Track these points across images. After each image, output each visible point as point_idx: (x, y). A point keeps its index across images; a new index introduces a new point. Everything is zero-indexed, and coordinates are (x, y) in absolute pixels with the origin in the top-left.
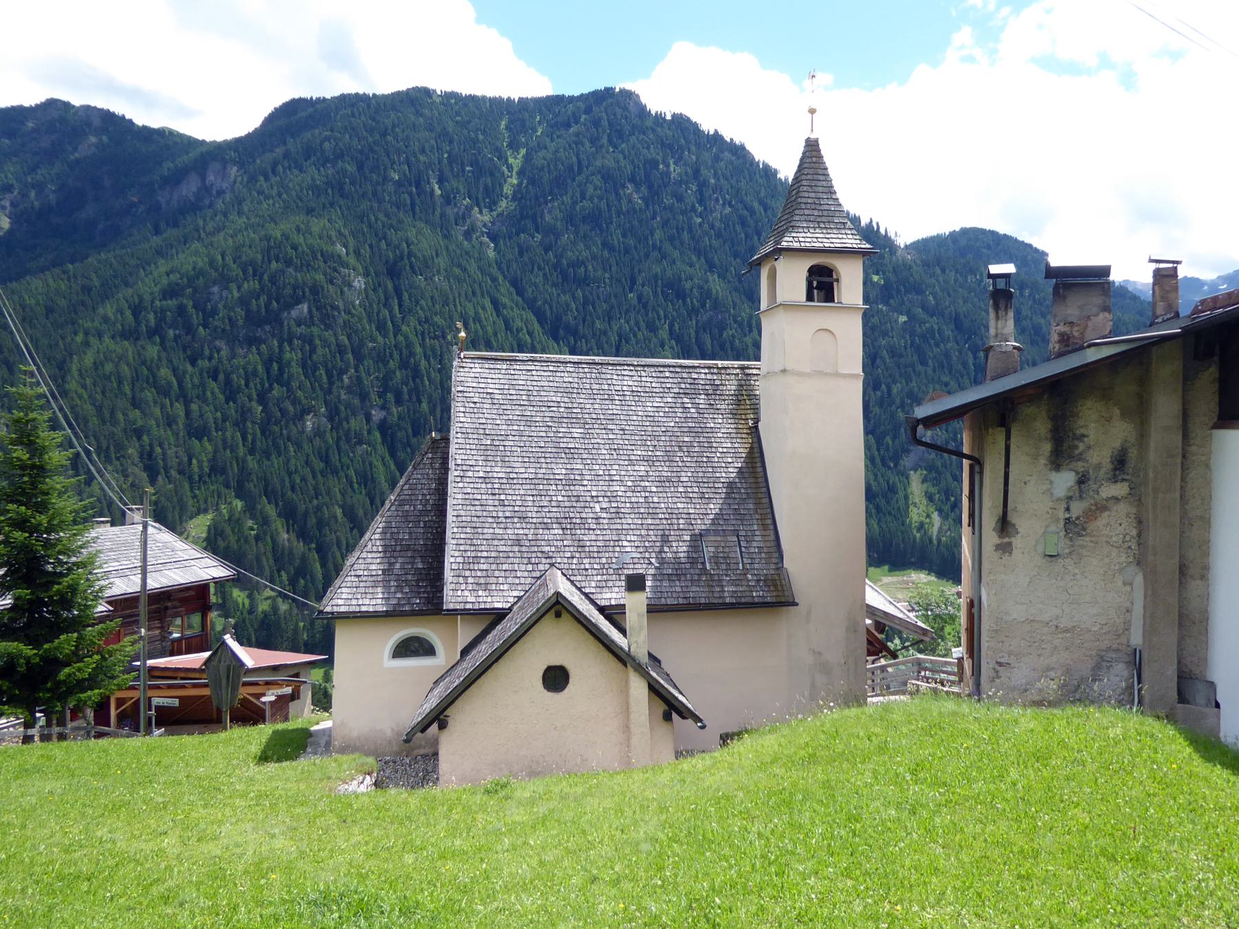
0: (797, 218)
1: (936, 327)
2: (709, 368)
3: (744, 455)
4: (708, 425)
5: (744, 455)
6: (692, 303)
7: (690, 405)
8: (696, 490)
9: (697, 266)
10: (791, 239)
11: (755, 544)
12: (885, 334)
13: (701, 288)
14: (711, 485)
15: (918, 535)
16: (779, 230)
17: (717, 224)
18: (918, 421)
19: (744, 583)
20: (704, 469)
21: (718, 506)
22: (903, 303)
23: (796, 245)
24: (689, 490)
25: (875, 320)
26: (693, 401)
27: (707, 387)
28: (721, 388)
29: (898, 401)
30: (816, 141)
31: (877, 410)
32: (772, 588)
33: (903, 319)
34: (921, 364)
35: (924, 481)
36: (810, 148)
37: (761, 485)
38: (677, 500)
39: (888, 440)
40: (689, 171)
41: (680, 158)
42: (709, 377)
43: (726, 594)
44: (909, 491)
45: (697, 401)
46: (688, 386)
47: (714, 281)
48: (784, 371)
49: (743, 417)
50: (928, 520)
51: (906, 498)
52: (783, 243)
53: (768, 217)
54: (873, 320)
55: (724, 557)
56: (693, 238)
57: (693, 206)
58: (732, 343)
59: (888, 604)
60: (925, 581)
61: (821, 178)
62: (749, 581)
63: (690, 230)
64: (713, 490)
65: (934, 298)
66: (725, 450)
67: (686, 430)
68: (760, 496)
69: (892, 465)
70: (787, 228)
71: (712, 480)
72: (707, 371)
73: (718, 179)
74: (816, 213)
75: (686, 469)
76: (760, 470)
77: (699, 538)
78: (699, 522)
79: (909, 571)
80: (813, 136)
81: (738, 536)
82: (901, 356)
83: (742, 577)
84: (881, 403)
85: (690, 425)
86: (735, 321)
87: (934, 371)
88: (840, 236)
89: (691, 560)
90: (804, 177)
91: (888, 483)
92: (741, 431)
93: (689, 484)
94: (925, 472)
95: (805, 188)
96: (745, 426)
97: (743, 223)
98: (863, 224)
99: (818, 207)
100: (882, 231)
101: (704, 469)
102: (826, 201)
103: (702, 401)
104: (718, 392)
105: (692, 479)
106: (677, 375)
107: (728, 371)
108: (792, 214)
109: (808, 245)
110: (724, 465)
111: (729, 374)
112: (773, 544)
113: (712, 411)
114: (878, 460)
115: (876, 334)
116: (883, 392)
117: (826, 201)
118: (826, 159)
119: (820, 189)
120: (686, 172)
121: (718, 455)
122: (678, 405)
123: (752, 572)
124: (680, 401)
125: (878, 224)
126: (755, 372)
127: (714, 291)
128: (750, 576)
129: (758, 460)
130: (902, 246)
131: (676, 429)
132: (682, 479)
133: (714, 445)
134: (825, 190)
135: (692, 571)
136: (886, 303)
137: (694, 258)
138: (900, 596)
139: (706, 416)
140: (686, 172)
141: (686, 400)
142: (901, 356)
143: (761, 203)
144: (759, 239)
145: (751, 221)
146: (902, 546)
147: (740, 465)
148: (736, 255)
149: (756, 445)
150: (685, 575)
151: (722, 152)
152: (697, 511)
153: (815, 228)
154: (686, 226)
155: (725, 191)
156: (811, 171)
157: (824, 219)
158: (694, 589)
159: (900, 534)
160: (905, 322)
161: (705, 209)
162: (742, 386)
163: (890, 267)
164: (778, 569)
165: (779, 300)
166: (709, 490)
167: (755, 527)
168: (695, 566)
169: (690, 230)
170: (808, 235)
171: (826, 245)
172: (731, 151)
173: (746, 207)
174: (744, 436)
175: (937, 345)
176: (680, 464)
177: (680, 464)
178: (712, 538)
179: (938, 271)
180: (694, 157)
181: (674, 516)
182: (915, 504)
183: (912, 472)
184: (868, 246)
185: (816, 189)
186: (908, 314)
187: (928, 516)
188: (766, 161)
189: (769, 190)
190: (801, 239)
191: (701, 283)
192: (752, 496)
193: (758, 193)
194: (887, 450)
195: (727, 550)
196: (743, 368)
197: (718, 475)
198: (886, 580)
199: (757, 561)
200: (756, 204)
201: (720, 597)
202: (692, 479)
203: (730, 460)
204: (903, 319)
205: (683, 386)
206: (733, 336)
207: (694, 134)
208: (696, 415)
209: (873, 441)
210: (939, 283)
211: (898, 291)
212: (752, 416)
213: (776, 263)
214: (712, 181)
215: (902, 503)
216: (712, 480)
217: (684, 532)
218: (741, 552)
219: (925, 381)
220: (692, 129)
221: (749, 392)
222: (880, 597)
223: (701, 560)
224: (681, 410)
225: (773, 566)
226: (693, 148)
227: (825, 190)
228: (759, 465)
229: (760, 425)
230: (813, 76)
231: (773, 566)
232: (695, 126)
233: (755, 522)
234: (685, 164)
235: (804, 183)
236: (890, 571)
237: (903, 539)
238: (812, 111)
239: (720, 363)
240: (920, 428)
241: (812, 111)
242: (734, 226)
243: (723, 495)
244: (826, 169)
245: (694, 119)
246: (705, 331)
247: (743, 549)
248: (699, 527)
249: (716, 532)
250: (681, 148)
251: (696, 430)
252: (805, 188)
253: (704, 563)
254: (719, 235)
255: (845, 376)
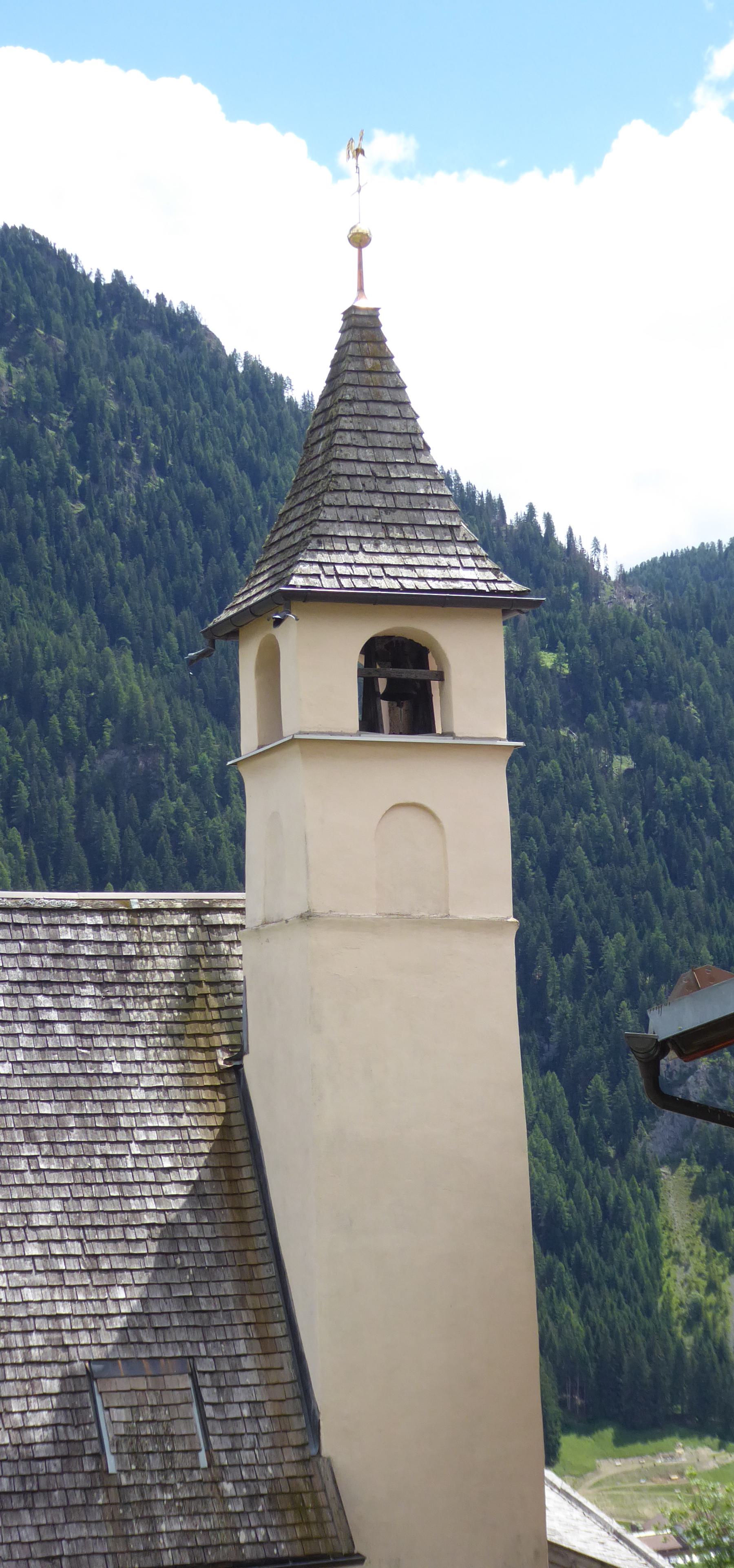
0: (330, 514)
1: (708, 784)
2: (106, 911)
3: (205, 1148)
4: (106, 1069)
5: (205, 1148)
6: (64, 727)
7: (54, 1015)
8: (75, 1248)
9: (77, 630)
10: (315, 569)
11: (240, 1395)
12: (578, 803)
13: (87, 687)
14: (116, 1234)
15: (688, 1341)
16: (284, 545)
17: (128, 519)
18: (663, 1047)
19: (214, 1506)
20: (95, 1191)
21: (137, 1292)
22: (622, 722)
23: (329, 584)
24: (57, 1250)
25: (551, 768)
26: (64, 1003)
27: (101, 964)
28: (139, 964)
29: (619, 980)
30: (373, 316)
31: (566, 1005)
32: (291, 1517)
33: (623, 763)
34: (674, 878)
35: (697, 1192)
36: (356, 335)
37: (254, 1229)
38: (21, 1280)
39: (599, 1083)
40: (50, 378)
41: (25, 346)
42: (106, 935)
43: (164, 1542)
44: (659, 1222)
45: (74, 1002)
46: (48, 962)
47: (124, 669)
48: (307, 917)
49: (202, 1042)
50: (712, 1299)
51: (653, 1238)
52: (295, 581)
53: (262, 500)
54: (547, 769)
55: (154, 1437)
56: (63, 554)
57: (62, 471)
58: (175, 834)
59: (611, 1543)
60: (712, 1465)
61: (390, 410)
62: (225, 1499)
63: (56, 533)
64: (122, 1248)
65: (701, 707)
66: (153, 1135)
67: (44, 1083)
68: (251, 1258)
69: (611, 1152)
70: (305, 542)
71: (118, 1220)
72: (99, 920)
73: (129, 400)
74: (378, 501)
75: (46, 1192)
76: (250, 1186)
77: (84, 1384)
78: (85, 1338)
79: (668, 1441)
80: (362, 304)
81: (193, 1375)
82: (622, 861)
83: (207, 1490)
84: (575, 987)
85: (56, 1068)
86: (184, 776)
87: (710, 899)
88: (444, 561)
89: (62, 1450)
90: (343, 408)
91: (603, 1200)
92: (197, 1081)
93: (56, 1234)
94: (698, 1169)
95: (348, 438)
96: (208, 1067)
97: (199, 519)
98: (511, 518)
99: (382, 486)
100: (561, 537)
101: (95, 1191)
102: (403, 471)
103: (87, 1003)
104: (132, 977)
105: (63, 1220)
106: (18, 934)
107: (158, 920)
108: (315, 503)
109: (360, 583)
110: (150, 1177)
111: (159, 928)
112: (290, 1391)
113: (116, 1029)
114: (574, 1140)
115: (557, 803)
116: (579, 957)
117: (403, 471)
118: (399, 362)
119: (388, 440)
120: (41, 382)
121: (135, 1149)
122: (22, 1016)
123: (234, 1474)
124: (25, 1003)
125: (548, 519)
126: (230, 919)
127: (124, 697)
128: (228, 1487)
129: (244, 1159)
130: (613, 576)
131: (16, 1082)
132: (36, 1221)
133: (124, 1122)
134: (400, 442)
135: (67, 1481)
136: (579, 724)
137: (68, 609)
138: (648, 1511)
139: (100, 1042)
140: (41, 382)
141: (43, 1001)
142: (622, 861)
143: (245, 464)
144: (241, 558)
145: (216, 509)
146: (647, 1370)
147: (194, 1175)
148: (180, 601)
149: (237, 1119)
150: (48, 1491)
151: (138, 331)
152: (79, 1310)
153: (376, 541)
154: (43, 523)
155: (147, 432)
156: (361, 394)
157: (400, 517)
158: (73, 1531)
159: (640, 1338)
160: (629, 772)
161: (95, 479)
162: (195, 957)
163: (583, 631)
164: (305, 1461)
165: (289, 729)
166: (111, 1249)
167: (241, 1347)
168: (75, 1465)
169: (56, 533)
170: (361, 558)
171: (409, 584)
172: (158, 328)
173: (203, 473)
174: (204, 1094)
175: (714, 831)
176: (30, 1178)
177: (30, 1178)
178: (123, 1384)
179: (708, 640)
180: (60, 342)
181: (15, 1326)
182: (676, 1255)
183: (665, 1170)
184: (515, 586)
185: (375, 439)
186: (636, 750)
187: (712, 1287)
188: (254, 354)
189: (261, 429)
190: (341, 570)
191: (89, 674)
192: (229, 1259)
193: (234, 438)
194: (597, 1110)
195: (163, 1414)
196: (196, 910)
197: (135, 1205)
198: (610, 1467)
199: (248, 1441)
200: (229, 467)
201: (147, 1551)
202: (63, 1220)
203: (167, 1163)
204: (623, 763)
205: (35, 962)
206: (178, 815)
207: (60, 280)
208: (70, 1042)
209: (560, 1089)
210: (712, 671)
211: (608, 694)
212: (225, 1040)
213: (279, 633)
214: (112, 406)
215: (642, 1251)
216: (118, 1220)
217: (43, 1370)
218: (203, 1419)
219: (686, 925)
220: (53, 269)
221: (213, 976)
222: (590, 1522)
223: (91, 1448)
224: (29, 1029)
225: (291, 1455)
226: (58, 319)
227: (400, 442)
228: (246, 1172)
229: (248, 1062)
230: (359, 151)
231: (291, 1455)
232: (63, 262)
233: (240, 1331)
234: (38, 361)
235: (345, 423)
236: (619, 1441)
237: (650, 1352)
238: (360, 240)
239: (136, 898)
240: (671, 1061)
241: (360, 240)
242: (173, 525)
243: (150, 1262)
244: (401, 388)
245: (59, 241)
246: (101, 803)
247: (209, 1411)
248: (84, 1353)
249: (133, 1366)
250: (25, 317)
251: (72, 1082)
252: (348, 438)
253: (99, 1456)
254: (133, 548)
255: (468, 926)
